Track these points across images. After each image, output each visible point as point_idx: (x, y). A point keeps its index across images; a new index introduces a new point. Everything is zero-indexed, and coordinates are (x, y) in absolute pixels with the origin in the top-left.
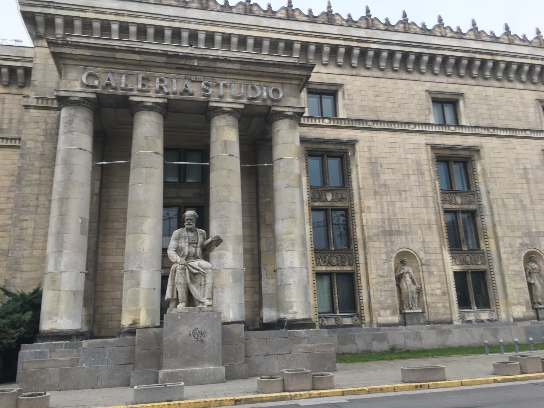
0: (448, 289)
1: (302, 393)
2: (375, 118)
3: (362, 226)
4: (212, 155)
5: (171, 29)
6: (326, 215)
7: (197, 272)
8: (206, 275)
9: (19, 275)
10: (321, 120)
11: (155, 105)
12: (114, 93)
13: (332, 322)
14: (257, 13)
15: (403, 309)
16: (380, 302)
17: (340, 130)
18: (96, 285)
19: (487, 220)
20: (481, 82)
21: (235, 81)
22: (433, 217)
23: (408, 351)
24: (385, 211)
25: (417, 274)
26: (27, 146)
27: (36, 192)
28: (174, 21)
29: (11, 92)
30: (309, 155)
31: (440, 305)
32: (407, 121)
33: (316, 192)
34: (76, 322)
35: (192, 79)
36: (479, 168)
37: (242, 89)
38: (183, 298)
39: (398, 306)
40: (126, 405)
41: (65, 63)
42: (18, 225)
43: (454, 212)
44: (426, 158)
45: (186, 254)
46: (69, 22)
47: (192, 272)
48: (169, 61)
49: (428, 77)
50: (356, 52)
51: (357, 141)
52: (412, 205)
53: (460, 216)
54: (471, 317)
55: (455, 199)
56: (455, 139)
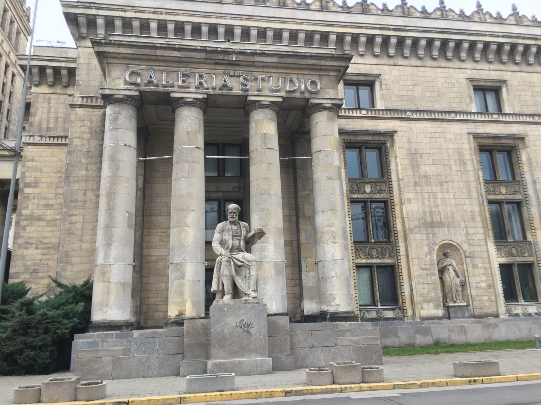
1: (353, 386)
2: (414, 108)
4: (251, 149)
5: (208, 25)
6: (364, 208)
7: (242, 264)
8: (251, 267)
9: (69, 267)
10: (358, 111)
12: (156, 90)
13: (374, 315)
14: (291, 6)
15: (447, 302)
16: (422, 295)
17: (378, 121)
18: (141, 277)
20: (525, 68)
21: (273, 75)
22: (476, 208)
23: (453, 345)
25: (460, 266)
26: (74, 144)
29: (56, 92)
30: (347, 147)
31: (486, 298)
32: (447, 110)
33: (355, 183)
35: (231, 74)
36: (524, 157)
38: (229, 290)
40: (179, 394)
41: (108, 61)
42: (68, 219)
43: (499, 203)
44: (468, 147)
45: (230, 246)
46: (110, 22)
47: (237, 264)
48: (208, 57)
49: (469, 64)
50: (394, 41)
51: (396, 132)
52: (454, 196)
53: (505, 206)
56: (498, 128)
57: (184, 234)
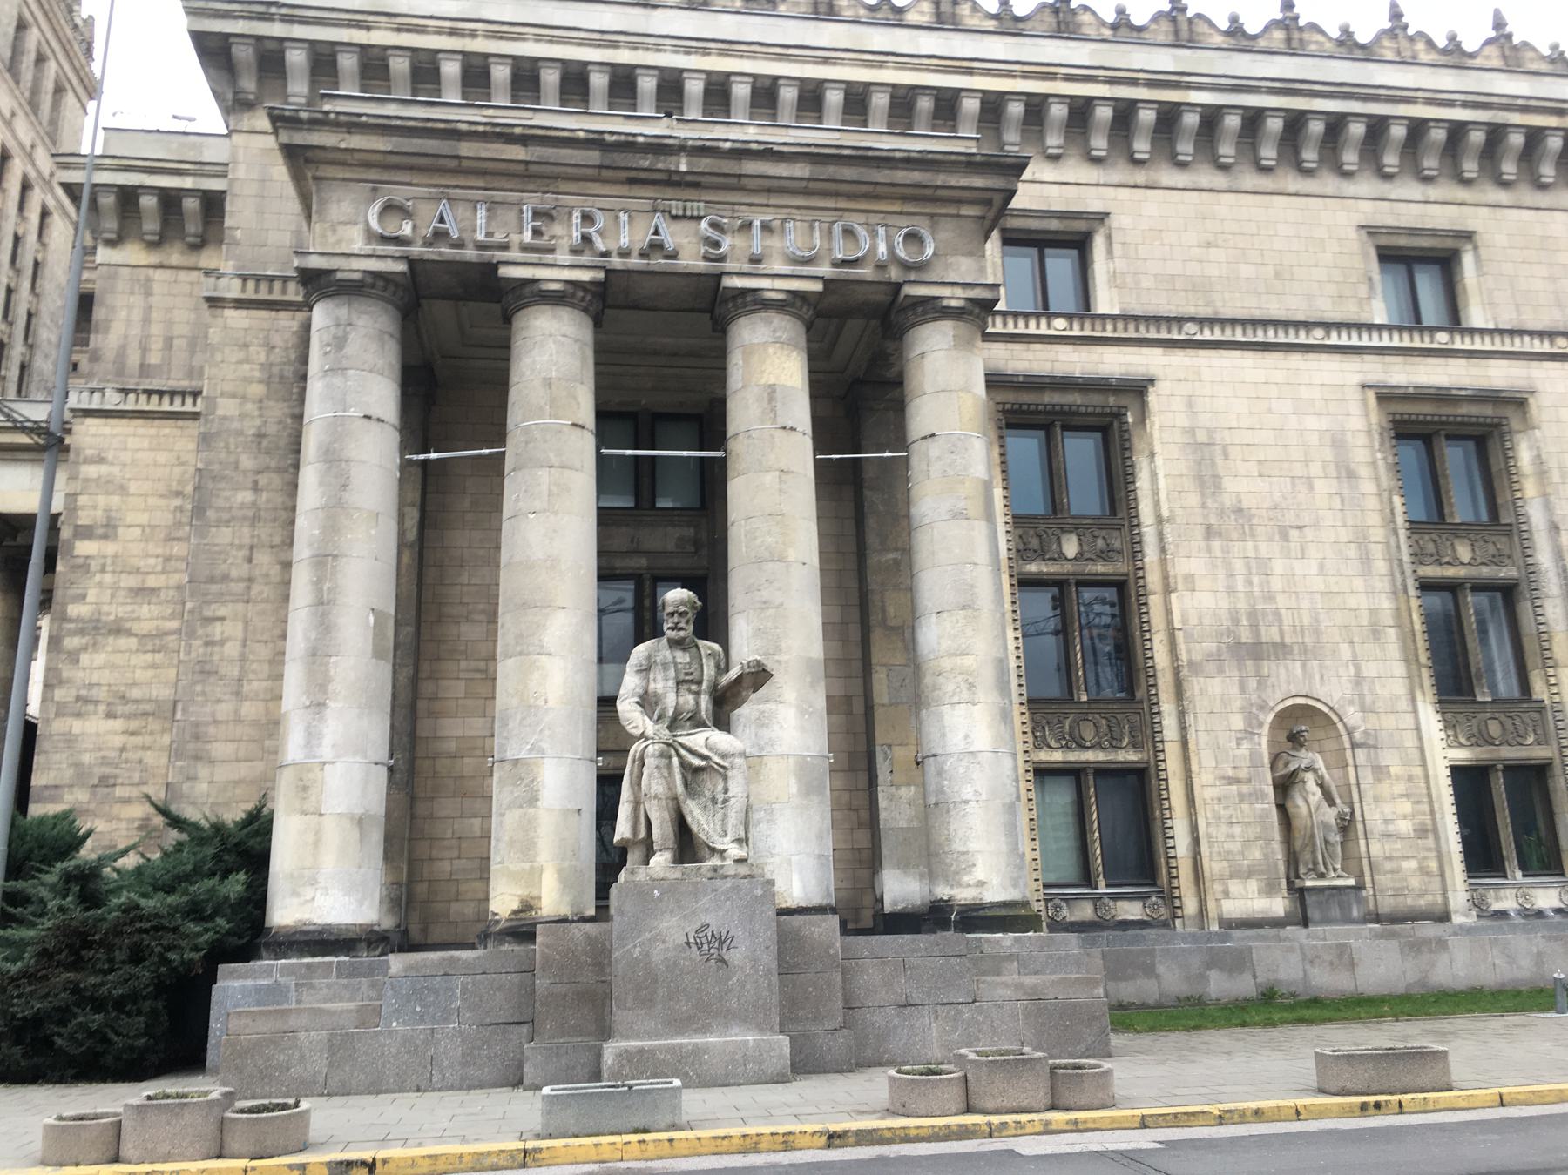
0: (1434, 820)
1: (1023, 1118)
3: (1171, 633)
4: (732, 428)
6: (1060, 603)
7: (703, 763)
8: (729, 773)
9: (203, 771)
10: (1043, 321)
11: (570, 289)
12: (458, 258)
13: (1085, 912)
15: (1298, 877)
16: (1227, 856)
18: (413, 799)
20: (1528, 196)
21: (796, 214)
22: (1386, 604)
23: (1315, 1001)
24: (1240, 584)
25: (1337, 773)
26: (220, 412)
27: (247, 541)
28: (617, 47)
29: (166, 263)
30: (1010, 426)
33: (1032, 530)
34: (367, 903)
35: (674, 212)
36: (1524, 456)
37: (817, 234)
38: (664, 838)
39: (1282, 868)
40: (520, 1139)
41: (318, 174)
42: (200, 632)
43: (1452, 588)
44: (1361, 426)
45: (670, 712)
46: (323, 61)
47: (690, 765)
48: (607, 162)
49: (1366, 185)
50: (1147, 116)
51: (1152, 381)
52: (1321, 567)
54: (1506, 901)
55: (1454, 550)
57: (536, 675)
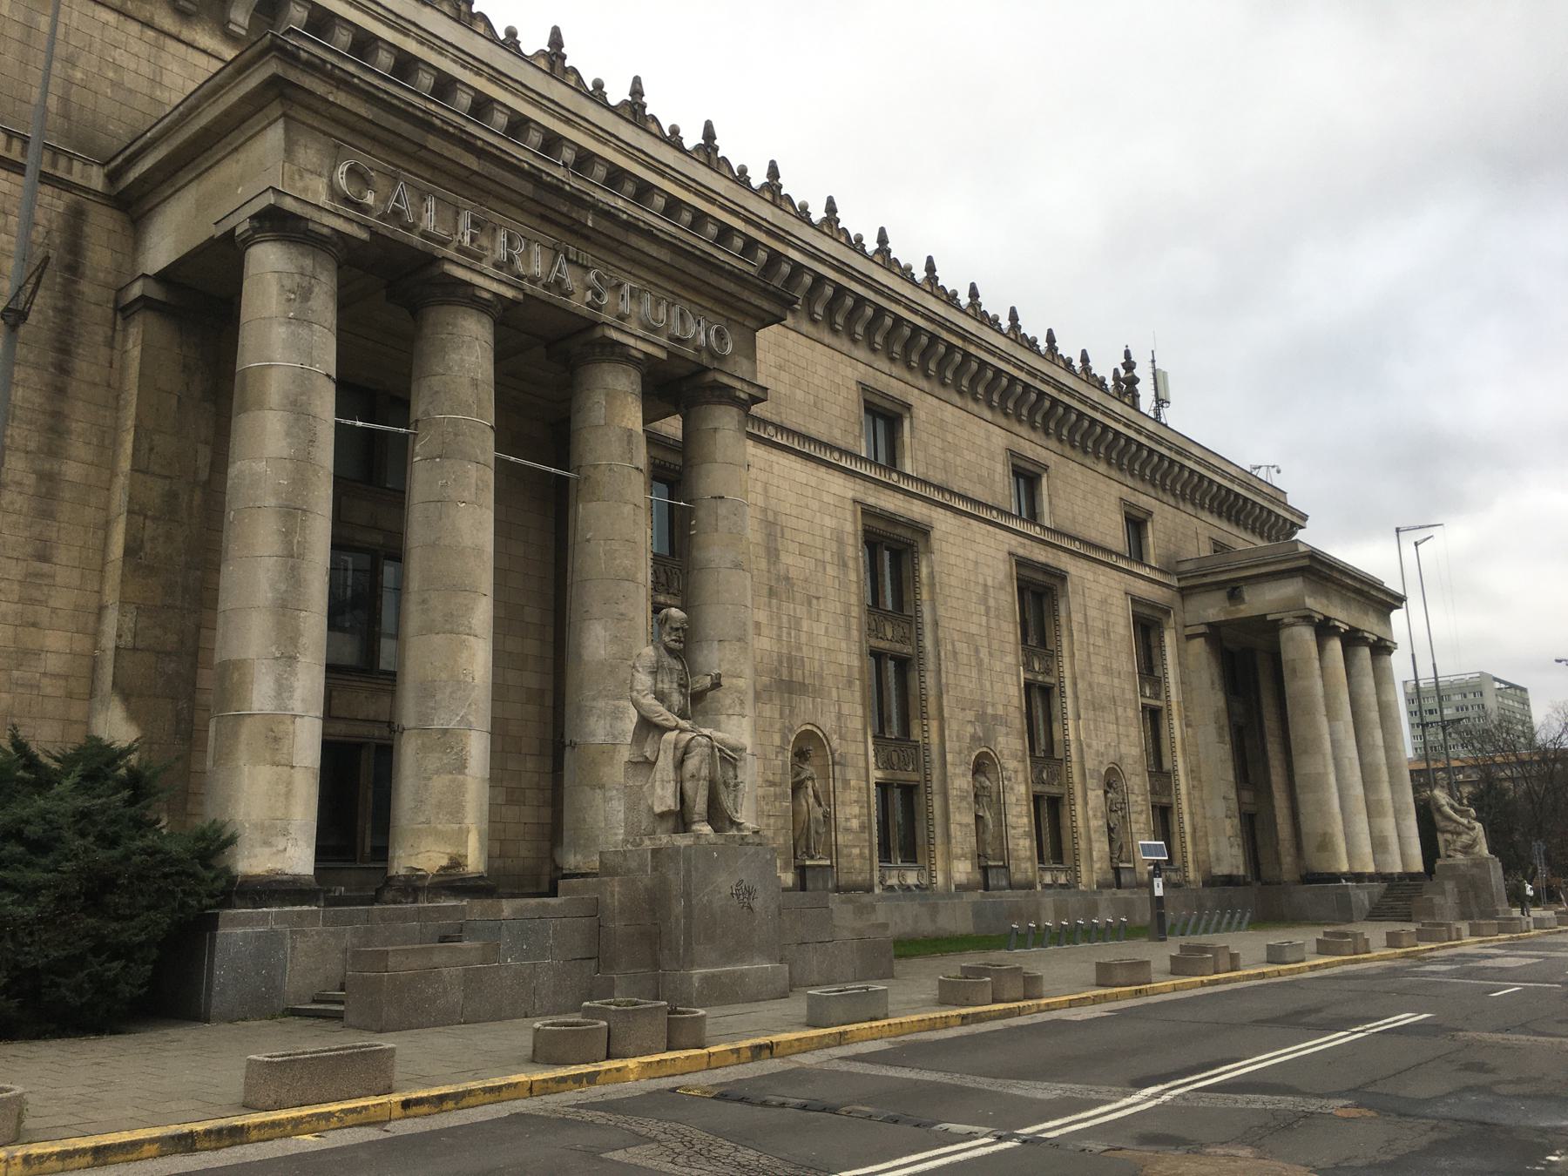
19: (930, 680)
22: (856, 663)
28: (407, 35)
31: (856, 851)
36: (924, 571)
41: (292, 113)
44: (850, 527)
57: (465, 654)
